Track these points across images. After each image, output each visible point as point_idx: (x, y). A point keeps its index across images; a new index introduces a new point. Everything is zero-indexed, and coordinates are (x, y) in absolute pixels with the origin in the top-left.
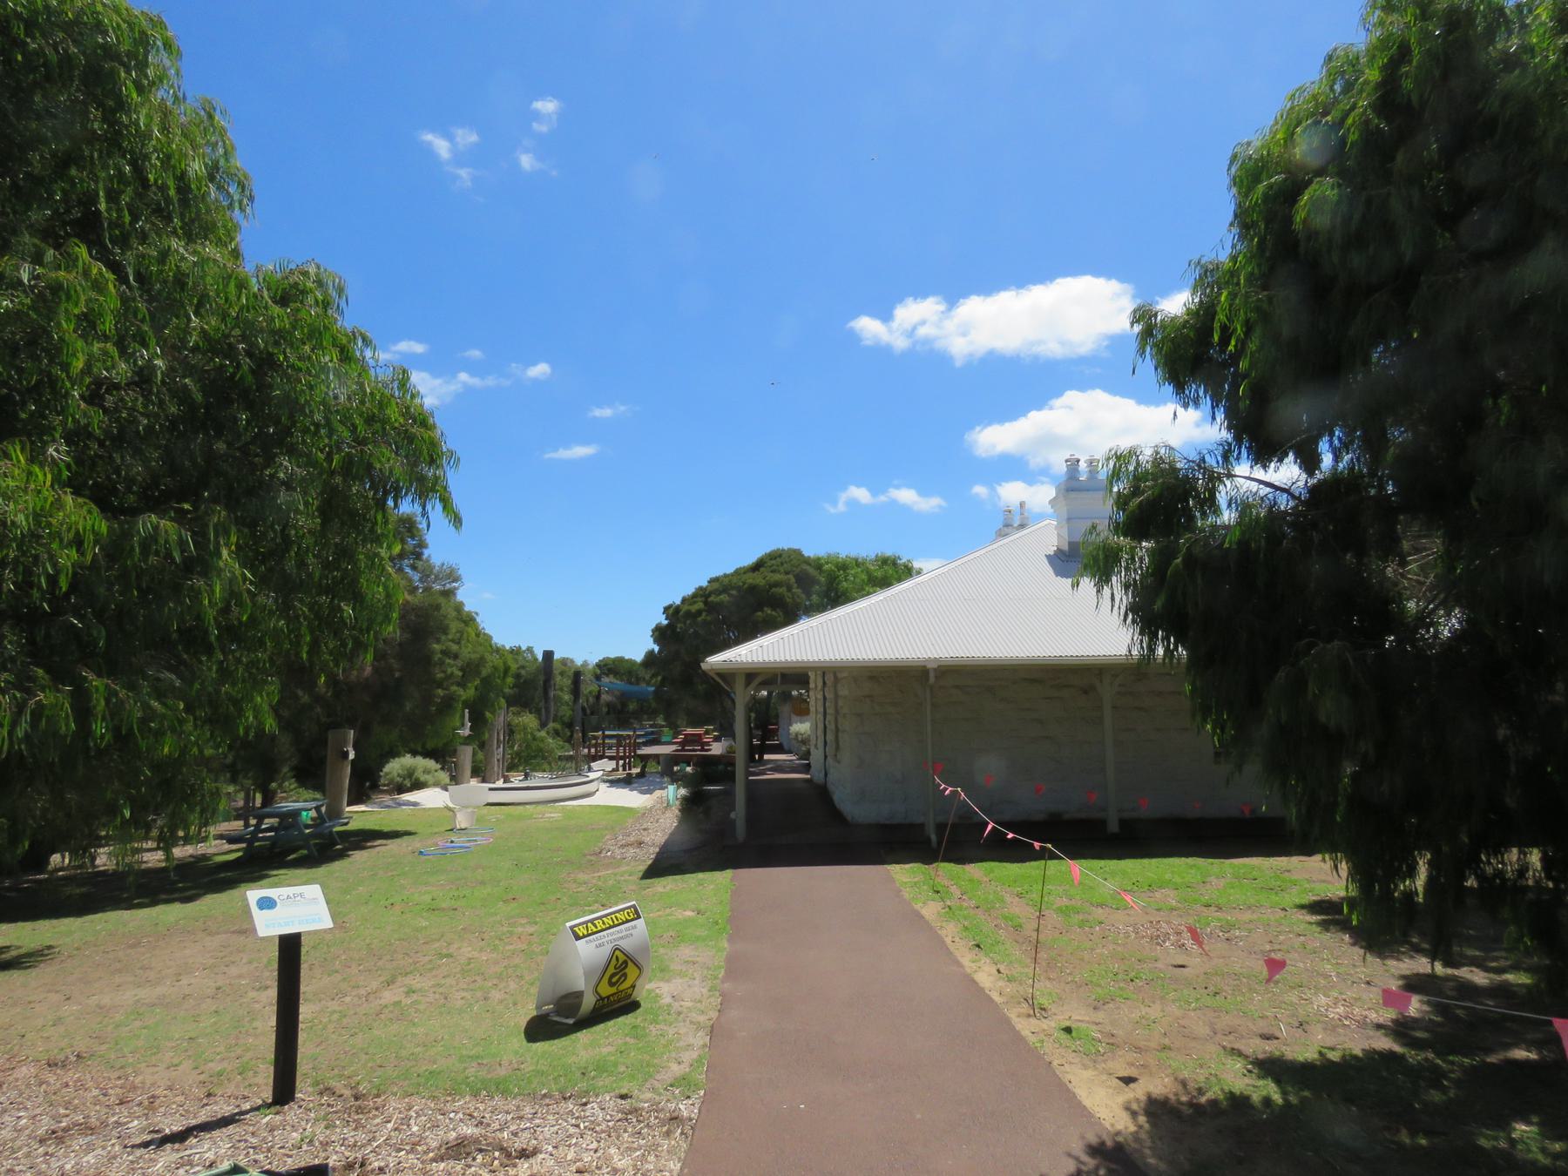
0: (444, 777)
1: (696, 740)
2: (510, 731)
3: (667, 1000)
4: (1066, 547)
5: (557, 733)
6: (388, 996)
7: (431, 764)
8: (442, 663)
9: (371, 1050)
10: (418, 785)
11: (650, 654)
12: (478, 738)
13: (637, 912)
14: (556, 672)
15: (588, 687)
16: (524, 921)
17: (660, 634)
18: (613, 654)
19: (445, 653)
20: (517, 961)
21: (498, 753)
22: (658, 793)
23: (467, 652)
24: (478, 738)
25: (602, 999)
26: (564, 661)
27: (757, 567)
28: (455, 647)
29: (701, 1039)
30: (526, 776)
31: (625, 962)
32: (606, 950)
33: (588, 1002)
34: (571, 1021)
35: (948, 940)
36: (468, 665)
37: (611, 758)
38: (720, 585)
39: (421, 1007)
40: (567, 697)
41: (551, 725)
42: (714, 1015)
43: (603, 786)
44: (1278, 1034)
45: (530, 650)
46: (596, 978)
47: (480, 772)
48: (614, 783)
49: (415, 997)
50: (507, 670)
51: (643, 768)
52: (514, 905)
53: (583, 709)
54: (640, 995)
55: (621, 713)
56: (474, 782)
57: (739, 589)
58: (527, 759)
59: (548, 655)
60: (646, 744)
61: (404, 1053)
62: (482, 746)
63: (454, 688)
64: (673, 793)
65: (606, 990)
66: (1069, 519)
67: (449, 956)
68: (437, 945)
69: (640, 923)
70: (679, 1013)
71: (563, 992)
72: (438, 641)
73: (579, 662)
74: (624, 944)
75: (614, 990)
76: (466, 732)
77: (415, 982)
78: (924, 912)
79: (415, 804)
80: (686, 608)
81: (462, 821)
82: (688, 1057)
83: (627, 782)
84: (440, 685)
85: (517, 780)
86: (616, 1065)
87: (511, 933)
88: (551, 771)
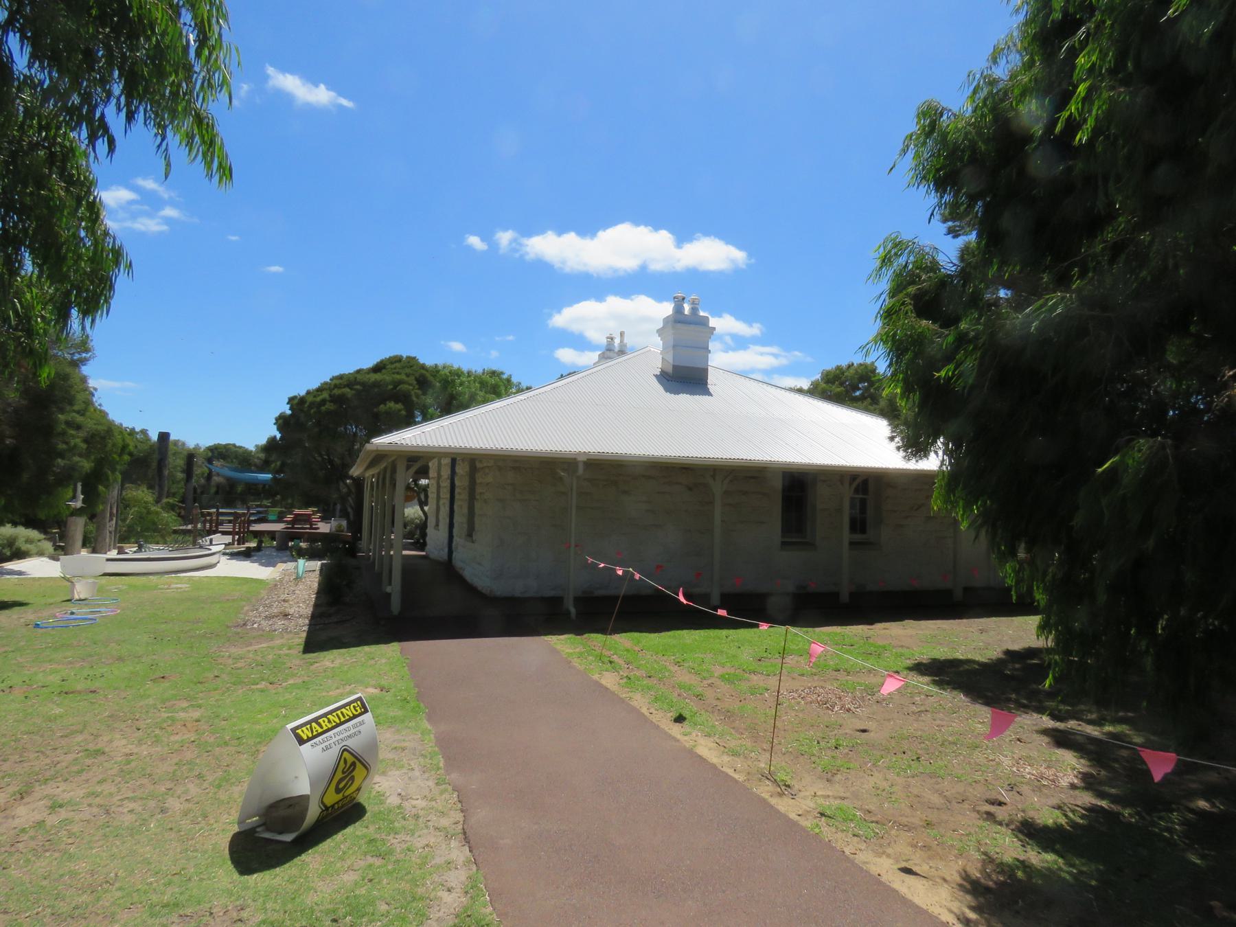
0: (48, 546)
1: (307, 519)
2: (124, 504)
3: (393, 800)
4: (670, 370)
5: (172, 507)
6: (25, 814)
7: (34, 534)
8: (64, 433)
9: (12, 906)
10: (20, 555)
11: (272, 440)
12: (90, 511)
13: (363, 706)
14: (170, 453)
15: (200, 469)
16: (185, 704)
17: (283, 422)
18: (223, 441)
19: (68, 423)
20: (189, 755)
21: (111, 525)
22: (281, 567)
23: (89, 424)
24: (90, 511)
25: (327, 808)
26: (176, 443)
27: (378, 368)
28: (79, 419)
29: (458, 852)
30: (140, 548)
31: (353, 764)
32: (335, 752)
33: (313, 812)
34: (288, 838)
35: (644, 710)
36: (93, 436)
37: (224, 533)
38: (342, 382)
39: (76, 828)
40: (180, 476)
41: (165, 500)
42: (459, 816)
43: (224, 559)
44: (1002, 800)
45: (144, 432)
46: (322, 789)
47: (92, 543)
48: (234, 555)
49: (63, 814)
50: (125, 447)
51: (260, 542)
52: (166, 684)
53: (195, 489)
54: (362, 799)
55: (230, 494)
56: (84, 552)
57: (363, 384)
58: (139, 532)
59: (164, 437)
60: (255, 522)
61: (63, 907)
62: (92, 517)
63: (76, 459)
64: (309, 570)
65: (332, 798)
66: (674, 346)
67: (100, 752)
68: (79, 738)
69: (368, 717)
70: (417, 817)
71: (272, 801)
72: (62, 411)
73: (191, 444)
74: (351, 743)
75: (340, 796)
76: (78, 504)
77: (61, 791)
78: (603, 682)
79: (20, 573)
80: (310, 399)
81: (81, 591)
82: (457, 878)
83: (247, 555)
84: (61, 455)
85: (131, 550)
86: (372, 903)
87: (173, 719)
88: (165, 543)
